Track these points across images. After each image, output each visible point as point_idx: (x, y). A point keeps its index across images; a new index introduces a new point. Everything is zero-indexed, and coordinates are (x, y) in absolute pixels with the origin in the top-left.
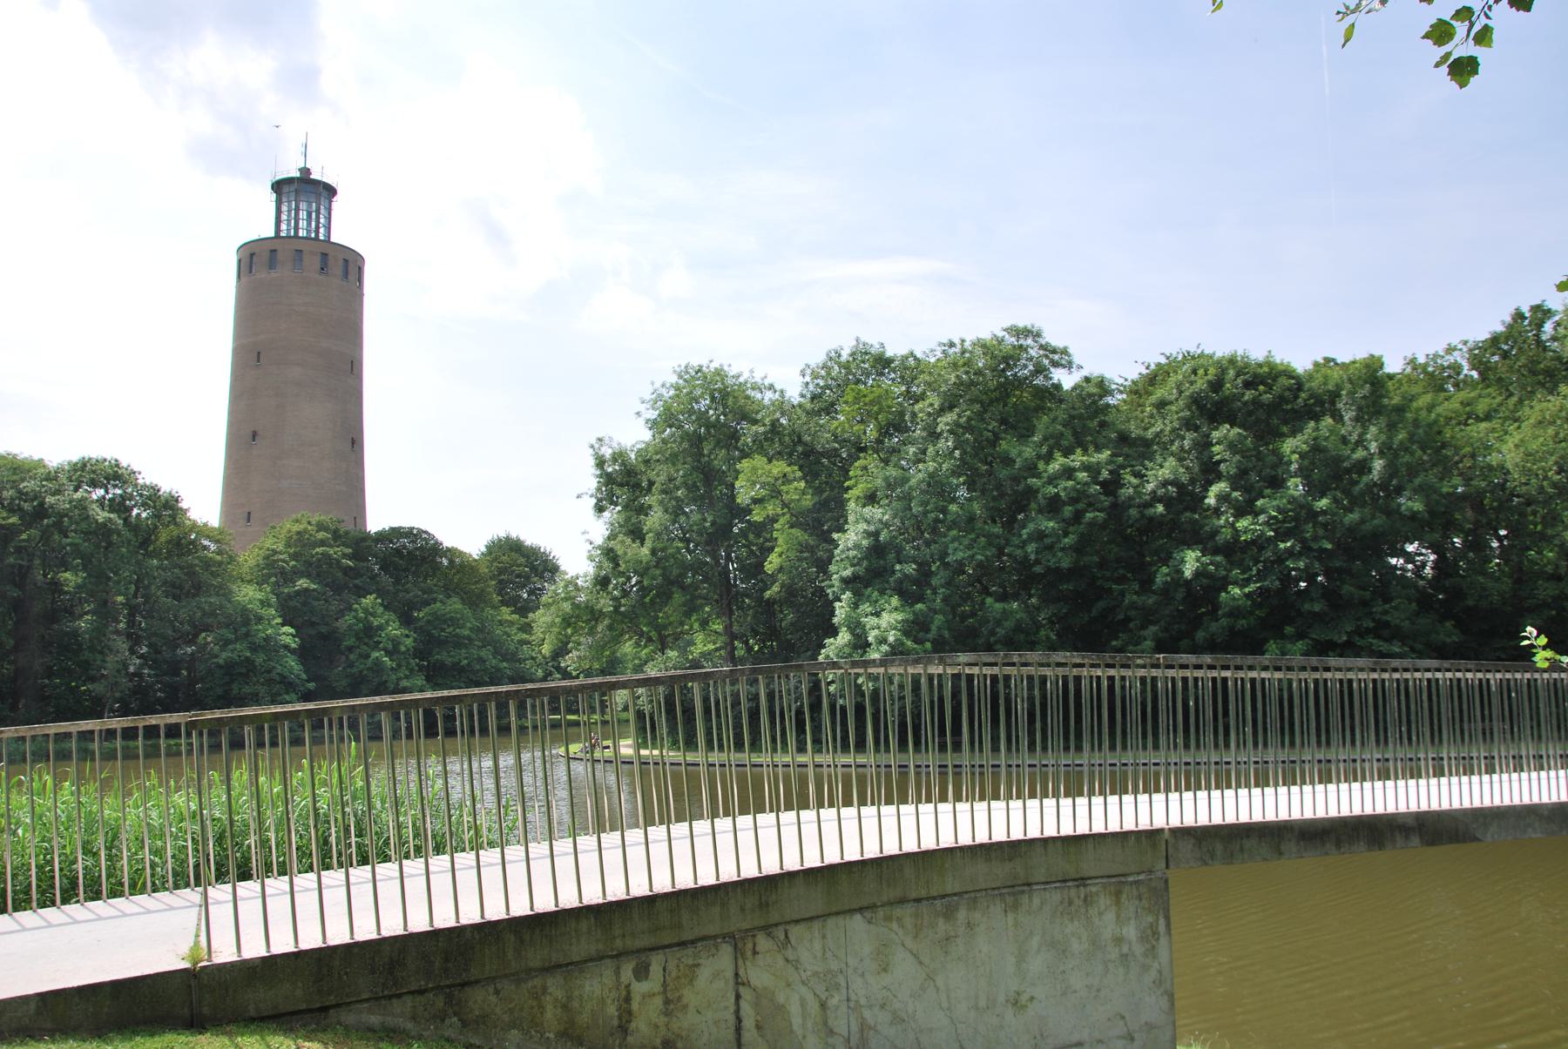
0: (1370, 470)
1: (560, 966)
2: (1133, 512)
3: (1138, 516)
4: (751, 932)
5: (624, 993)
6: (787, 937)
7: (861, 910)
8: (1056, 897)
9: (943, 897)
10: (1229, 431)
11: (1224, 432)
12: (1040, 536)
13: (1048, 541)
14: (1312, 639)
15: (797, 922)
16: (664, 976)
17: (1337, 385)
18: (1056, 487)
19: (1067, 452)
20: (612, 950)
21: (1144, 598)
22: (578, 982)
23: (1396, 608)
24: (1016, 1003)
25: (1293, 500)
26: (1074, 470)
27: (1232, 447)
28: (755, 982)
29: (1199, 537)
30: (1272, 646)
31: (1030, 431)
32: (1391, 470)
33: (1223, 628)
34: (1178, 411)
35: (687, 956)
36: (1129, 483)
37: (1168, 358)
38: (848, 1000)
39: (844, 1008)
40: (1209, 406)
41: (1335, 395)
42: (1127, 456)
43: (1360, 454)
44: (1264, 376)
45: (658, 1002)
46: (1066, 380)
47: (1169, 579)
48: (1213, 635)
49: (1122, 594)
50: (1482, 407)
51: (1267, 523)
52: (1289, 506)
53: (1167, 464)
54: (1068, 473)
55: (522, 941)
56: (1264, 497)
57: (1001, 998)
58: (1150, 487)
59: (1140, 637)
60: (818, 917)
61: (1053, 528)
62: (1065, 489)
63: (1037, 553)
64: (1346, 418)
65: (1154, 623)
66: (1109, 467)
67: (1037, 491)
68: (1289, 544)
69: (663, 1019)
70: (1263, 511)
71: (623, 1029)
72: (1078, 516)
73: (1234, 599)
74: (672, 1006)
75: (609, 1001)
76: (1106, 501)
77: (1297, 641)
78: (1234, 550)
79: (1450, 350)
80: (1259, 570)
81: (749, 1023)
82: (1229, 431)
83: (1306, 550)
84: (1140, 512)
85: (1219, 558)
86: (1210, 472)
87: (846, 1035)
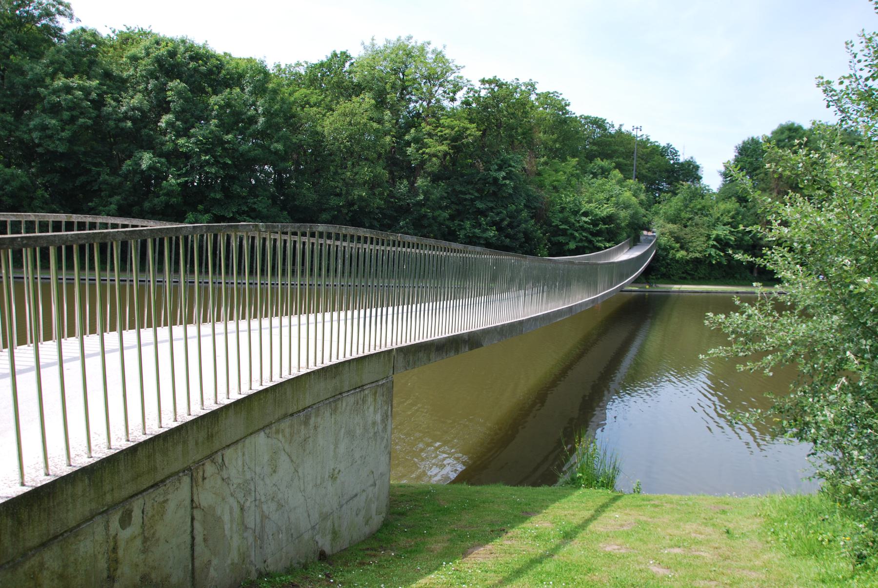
0: (256, 123)
1: (56, 537)
2: (111, 123)
3: (114, 126)
4: (200, 463)
5: (112, 544)
6: (223, 460)
7: (263, 429)
8: (351, 400)
9: (304, 410)
10: (179, 84)
11: (175, 84)
12: (44, 128)
13: (49, 132)
14: (212, 213)
15: (228, 446)
16: (143, 518)
17: (244, 70)
18: (59, 97)
19: (68, 75)
20: (103, 506)
21: (112, 178)
22: (74, 547)
23: (260, 202)
24: (333, 478)
25: (212, 132)
26: (72, 88)
27: (179, 94)
28: (204, 504)
29: (149, 145)
30: (190, 216)
31: (41, 55)
32: (268, 124)
33: (162, 202)
34: (146, 64)
35: (158, 495)
36: (110, 104)
37: (128, 29)
38: (255, 500)
39: (253, 508)
40: (167, 66)
41: (241, 76)
42: (109, 86)
43: (252, 112)
44: (199, 55)
45: (138, 542)
46: (67, 26)
47: (131, 168)
48: (155, 205)
49: (99, 174)
50: (313, 99)
51: (195, 143)
52: (210, 136)
53: (136, 97)
54: (68, 89)
55: (20, 523)
56: (194, 127)
57: (327, 476)
58: (124, 109)
59: (107, 202)
60: (241, 439)
61: (54, 125)
62: (65, 100)
63: (40, 139)
64: (246, 90)
65: (116, 194)
66: (97, 92)
67: (45, 98)
68: (207, 158)
69: (142, 557)
70: (193, 136)
71: (111, 578)
72: (73, 120)
73: (171, 185)
74: (148, 543)
75: (100, 556)
76: (94, 113)
77: (204, 214)
78: (175, 157)
79: (298, 64)
80: (187, 170)
81: (199, 539)
82: (179, 84)
83: (217, 162)
84: (115, 124)
85: (163, 160)
86: (163, 107)
87: (253, 527)
